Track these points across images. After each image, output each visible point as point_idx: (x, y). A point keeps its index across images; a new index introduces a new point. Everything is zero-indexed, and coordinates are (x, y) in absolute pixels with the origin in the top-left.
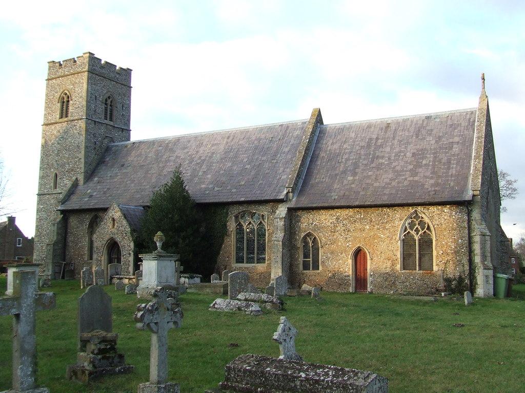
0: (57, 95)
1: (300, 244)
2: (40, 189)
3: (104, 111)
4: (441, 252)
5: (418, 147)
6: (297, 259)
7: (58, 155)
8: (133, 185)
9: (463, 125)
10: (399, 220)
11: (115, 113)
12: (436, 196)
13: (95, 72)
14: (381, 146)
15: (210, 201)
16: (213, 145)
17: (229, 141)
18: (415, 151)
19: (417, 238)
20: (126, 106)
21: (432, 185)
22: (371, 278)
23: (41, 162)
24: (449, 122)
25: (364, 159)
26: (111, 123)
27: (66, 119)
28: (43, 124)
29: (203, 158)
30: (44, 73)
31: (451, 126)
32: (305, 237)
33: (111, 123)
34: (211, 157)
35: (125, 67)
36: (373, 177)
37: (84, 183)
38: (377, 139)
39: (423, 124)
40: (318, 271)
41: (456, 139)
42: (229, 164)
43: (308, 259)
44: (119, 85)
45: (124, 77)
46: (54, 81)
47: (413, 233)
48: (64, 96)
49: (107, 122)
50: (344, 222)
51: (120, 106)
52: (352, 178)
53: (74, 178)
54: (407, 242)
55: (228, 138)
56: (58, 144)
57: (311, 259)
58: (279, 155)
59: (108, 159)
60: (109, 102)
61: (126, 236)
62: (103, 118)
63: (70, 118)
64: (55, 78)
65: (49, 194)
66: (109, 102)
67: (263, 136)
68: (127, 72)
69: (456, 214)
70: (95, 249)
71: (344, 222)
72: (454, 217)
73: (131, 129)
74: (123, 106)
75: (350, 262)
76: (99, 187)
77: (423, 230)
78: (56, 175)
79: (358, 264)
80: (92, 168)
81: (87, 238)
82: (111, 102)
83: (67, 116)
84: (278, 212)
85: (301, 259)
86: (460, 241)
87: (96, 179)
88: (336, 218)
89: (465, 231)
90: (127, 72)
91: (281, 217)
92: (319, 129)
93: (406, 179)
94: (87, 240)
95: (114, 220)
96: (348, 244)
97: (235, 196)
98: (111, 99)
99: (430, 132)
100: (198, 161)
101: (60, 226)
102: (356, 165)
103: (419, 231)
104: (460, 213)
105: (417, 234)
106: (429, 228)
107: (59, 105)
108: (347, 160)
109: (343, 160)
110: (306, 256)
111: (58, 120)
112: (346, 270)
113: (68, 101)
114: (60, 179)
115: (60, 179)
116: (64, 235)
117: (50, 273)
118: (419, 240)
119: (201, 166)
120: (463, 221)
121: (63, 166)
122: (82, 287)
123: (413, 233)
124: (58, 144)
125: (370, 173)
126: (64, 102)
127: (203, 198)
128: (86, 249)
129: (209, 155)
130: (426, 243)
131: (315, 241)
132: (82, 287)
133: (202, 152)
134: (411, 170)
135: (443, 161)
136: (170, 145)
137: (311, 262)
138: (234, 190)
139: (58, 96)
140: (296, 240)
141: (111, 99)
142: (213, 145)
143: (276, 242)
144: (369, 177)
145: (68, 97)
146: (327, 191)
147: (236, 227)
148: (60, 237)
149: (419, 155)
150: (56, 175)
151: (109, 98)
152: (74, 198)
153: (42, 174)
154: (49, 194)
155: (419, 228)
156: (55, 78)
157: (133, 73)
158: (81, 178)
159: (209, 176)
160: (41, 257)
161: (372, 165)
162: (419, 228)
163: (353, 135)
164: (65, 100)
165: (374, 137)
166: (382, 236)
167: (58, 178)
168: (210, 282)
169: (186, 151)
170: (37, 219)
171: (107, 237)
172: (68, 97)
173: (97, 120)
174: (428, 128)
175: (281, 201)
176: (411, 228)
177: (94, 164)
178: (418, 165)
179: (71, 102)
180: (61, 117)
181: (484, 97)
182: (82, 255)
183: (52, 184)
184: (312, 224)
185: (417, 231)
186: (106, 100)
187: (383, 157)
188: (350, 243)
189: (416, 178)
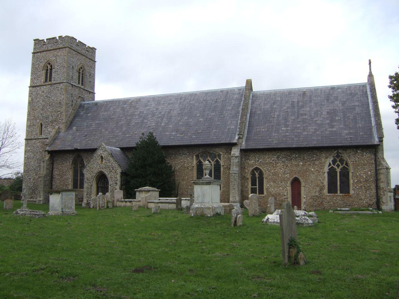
0: (42, 65)
1: (249, 176)
2: (27, 135)
3: (78, 77)
4: (356, 181)
5: (330, 108)
6: (246, 187)
7: (43, 109)
8: (107, 132)
9: (359, 94)
10: (327, 162)
11: (85, 80)
12: (352, 141)
13: (72, 48)
14: (302, 107)
15: (177, 144)
16: (169, 104)
17: (182, 101)
18: (328, 111)
19: (338, 170)
20: (92, 75)
21: (347, 134)
22: (304, 200)
23: (28, 115)
24: (349, 92)
25: (291, 116)
26: (82, 87)
27: (50, 83)
28: (29, 86)
29: (162, 113)
30: (31, 49)
31: (351, 94)
32: (253, 171)
33: (82, 87)
34: (169, 113)
35: (91, 46)
36: (302, 128)
37: (66, 131)
38: (298, 102)
39: (329, 92)
40: (263, 195)
41: (357, 104)
42: (186, 118)
43: (339, 192)
44: (88, 59)
45: (91, 54)
46: (39, 54)
47: (335, 167)
48: (48, 65)
49: (80, 85)
50: (283, 160)
51: (88, 75)
52: (285, 129)
53: (57, 127)
54: (332, 173)
55: (181, 99)
56: (43, 101)
57: (257, 187)
58: (225, 112)
59: (82, 113)
60: (81, 71)
61: (113, 170)
62: (77, 83)
63: (53, 82)
64: (40, 52)
65: (35, 139)
66: (81, 71)
67: (208, 98)
68: (93, 50)
69: (366, 154)
70: (86, 180)
71: (283, 160)
72: (365, 156)
73: (95, 92)
74: (90, 75)
75: (289, 188)
76: (78, 134)
77: (342, 165)
78: (41, 125)
79: (138, 202)
80: (70, 120)
81: (71, 172)
82: (83, 71)
83: (50, 80)
84: (232, 153)
85: (250, 186)
86: (369, 173)
87: (74, 128)
88: (277, 157)
89: (373, 166)
90: (93, 50)
91: (236, 156)
92: (252, 94)
93: (326, 130)
94: (71, 173)
95: (102, 158)
96: (286, 176)
97: (196, 141)
98: (82, 69)
99: (336, 98)
100: (159, 115)
101: (48, 163)
102: (286, 119)
103: (339, 166)
104: (369, 153)
105: (338, 168)
106: (347, 164)
107: (44, 72)
108: (278, 116)
109: (276, 116)
110: (254, 183)
111: (42, 84)
112: (285, 194)
113: (51, 69)
114: (45, 127)
115: (45, 127)
116: (51, 170)
117: (41, 199)
118: (340, 172)
119: (162, 119)
120: (372, 159)
121: (47, 118)
122: (98, 209)
123: (335, 167)
124: (43, 101)
125: (298, 126)
126: (47, 70)
127: (170, 142)
128: (70, 180)
129: (167, 111)
130: (345, 174)
131: (261, 174)
132: (98, 209)
133: (160, 109)
134: (328, 124)
135: (351, 118)
136: (133, 103)
137: (258, 189)
138: (194, 137)
139: (43, 66)
140: (245, 173)
141: (82, 69)
142: (169, 104)
143: (233, 175)
144: (298, 128)
145: (51, 66)
146: (268, 137)
147: (197, 163)
148: (48, 171)
149: (332, 114)
150: (41, 125)
151: (81, 68)
152: (58, 142)
153: (29, 124)
154: (35, 139)
155: (340, 164)
156: (40, 52)
157: (97, 51)
158: (62, 126)
159: (171, 126)
160: (29, 186)
161: (298, 120)
162: (340, 164)
163: (279, 99)
164: (49, 67)
165: (296, 100)
166: (312, 169)
167: (43, 127)
168: (349, 192)
169: (148, 108)
170: (25, 158)
171: (96, 171)
172: (51, 66)
173: (74, 84)
174: (335, 95)
175: (235, 144)
176: (334, 164)
177: (72, 117)
178: (332, 120)
179: (53, 70)
180: (46, 81)
181: (371, 76)
182: (66, 185)
183: (38, 132)
184: (258, 161)
185: (338, 166)
186: (79, 70)
187: (305, 114)
188: (288, 175)
189: (334, 129)
